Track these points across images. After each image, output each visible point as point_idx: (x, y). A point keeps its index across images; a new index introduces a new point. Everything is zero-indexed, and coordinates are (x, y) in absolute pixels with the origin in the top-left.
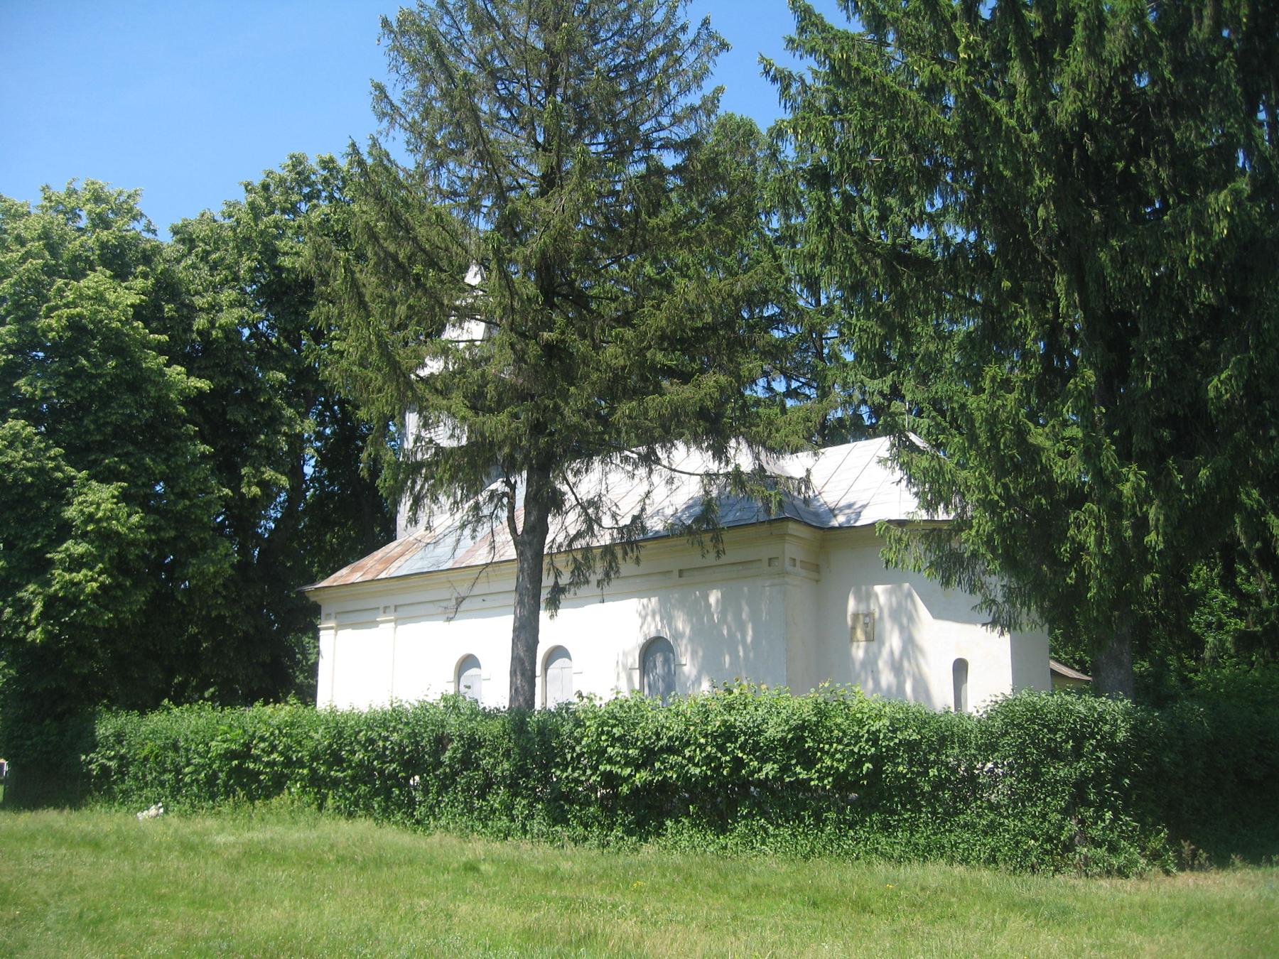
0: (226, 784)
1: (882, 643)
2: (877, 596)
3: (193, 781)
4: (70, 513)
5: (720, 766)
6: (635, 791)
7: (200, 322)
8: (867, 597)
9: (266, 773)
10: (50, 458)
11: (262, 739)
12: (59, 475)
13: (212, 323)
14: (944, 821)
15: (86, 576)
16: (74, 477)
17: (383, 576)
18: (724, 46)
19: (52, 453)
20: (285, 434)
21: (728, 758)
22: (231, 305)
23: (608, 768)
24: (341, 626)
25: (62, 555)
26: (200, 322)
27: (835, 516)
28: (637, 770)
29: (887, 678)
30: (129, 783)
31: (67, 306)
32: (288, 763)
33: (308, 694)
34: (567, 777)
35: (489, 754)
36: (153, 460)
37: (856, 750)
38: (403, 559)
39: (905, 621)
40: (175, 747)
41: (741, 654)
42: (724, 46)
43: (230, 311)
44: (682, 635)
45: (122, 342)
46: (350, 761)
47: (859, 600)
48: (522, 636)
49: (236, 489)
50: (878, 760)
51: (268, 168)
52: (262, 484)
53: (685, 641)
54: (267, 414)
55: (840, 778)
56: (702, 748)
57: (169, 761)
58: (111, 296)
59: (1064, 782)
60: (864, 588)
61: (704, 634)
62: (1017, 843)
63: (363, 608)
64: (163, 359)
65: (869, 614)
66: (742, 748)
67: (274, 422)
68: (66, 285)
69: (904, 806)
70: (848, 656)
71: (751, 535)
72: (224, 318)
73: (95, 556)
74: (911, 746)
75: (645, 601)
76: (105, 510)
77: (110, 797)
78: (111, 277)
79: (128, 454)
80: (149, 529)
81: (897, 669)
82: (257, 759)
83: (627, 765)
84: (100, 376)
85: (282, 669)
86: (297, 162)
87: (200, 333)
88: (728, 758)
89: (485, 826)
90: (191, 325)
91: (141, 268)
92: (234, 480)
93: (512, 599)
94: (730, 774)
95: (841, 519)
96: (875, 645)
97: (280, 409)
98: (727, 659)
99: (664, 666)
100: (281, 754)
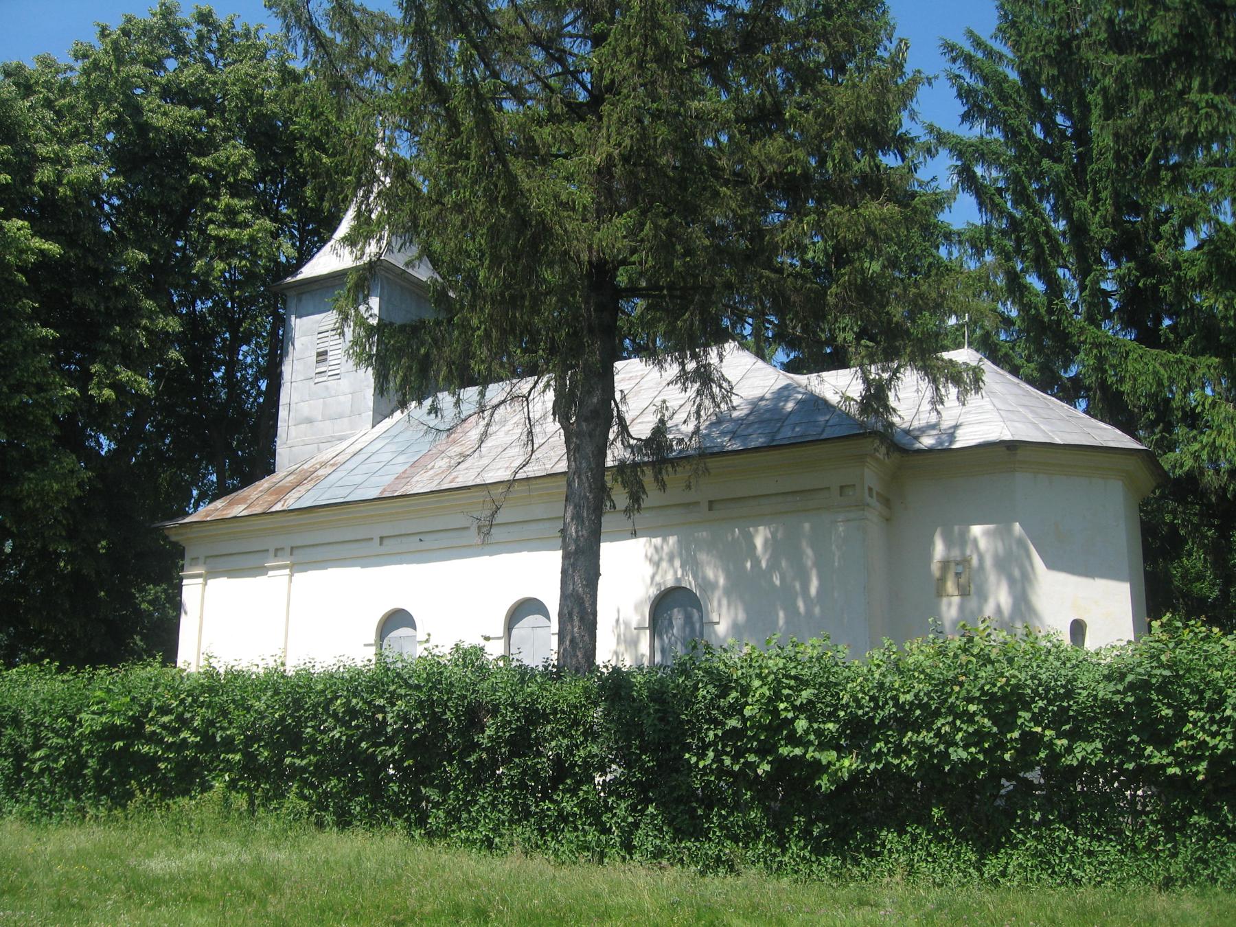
0: (97, 775)
1: (983, 597)
2: (975, 541)
3: (42, 771)
6: (844, 787)
7: (45, 174)
8: (959, 540)
11: (164, 710)
13: (59, 176)
20: (145, 328)
22: (81, 162)
24: (212, 574)
26: (45, 174)
32: (208, 743)
33: (170, 655)
38: (302, 489)
39: (1017, 573)
43: (87, 167)
46: (315, 742)
49: (84, 390)
52: (117, 386)
53: (718, 594)
54: (122, 303)
60: (956, 528)
63: (242, 553)
66: (1036, 720)
67: (130, 315)
82: (153, 739)
83: (822, 747)
86: (167, 12)
87: (42, 185)
90: (31, 177)
92: (83, 379)
95: (927, 441)
100: (195, 732)
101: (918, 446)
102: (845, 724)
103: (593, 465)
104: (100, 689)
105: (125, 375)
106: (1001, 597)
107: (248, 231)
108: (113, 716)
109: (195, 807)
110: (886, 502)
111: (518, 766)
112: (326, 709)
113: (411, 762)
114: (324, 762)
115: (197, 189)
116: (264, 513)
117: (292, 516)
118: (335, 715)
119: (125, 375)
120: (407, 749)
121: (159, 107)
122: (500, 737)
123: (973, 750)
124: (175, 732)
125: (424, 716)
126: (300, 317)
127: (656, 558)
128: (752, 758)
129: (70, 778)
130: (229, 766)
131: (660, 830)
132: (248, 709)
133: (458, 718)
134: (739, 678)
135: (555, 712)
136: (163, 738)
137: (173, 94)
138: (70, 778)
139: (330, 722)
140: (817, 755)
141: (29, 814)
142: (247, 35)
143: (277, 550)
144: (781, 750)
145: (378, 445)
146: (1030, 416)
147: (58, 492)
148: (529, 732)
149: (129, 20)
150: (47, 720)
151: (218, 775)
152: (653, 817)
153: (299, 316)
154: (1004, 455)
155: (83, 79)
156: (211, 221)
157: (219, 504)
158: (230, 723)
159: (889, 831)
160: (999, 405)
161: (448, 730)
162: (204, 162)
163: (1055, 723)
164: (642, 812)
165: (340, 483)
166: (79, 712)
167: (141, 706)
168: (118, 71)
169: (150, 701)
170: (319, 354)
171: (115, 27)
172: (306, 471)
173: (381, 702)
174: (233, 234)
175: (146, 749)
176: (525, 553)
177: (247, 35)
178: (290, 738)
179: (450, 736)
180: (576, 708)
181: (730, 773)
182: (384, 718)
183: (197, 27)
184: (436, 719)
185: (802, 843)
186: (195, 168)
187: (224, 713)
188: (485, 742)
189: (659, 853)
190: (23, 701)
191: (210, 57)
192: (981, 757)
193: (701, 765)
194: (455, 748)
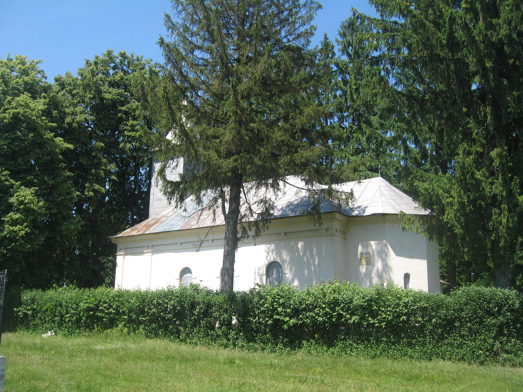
0: (85, 322)
1: (373, 266)
2: (371, 245)
3: (69, 321)
4: (13, 200)
5: (332, 317)
6: (290, 328)
7: (68, 119)
8: (367, 246)
10: (3, 175)
11: (105, 302)
12: (7, 183)
14: (438, 342)
15: (19, 228)
16: (14, 185)
18: (320, 7)
19: (4, 173)
20: (103, 170)
21: (336, 314)
22: (81, 113)
23: (278, 317)
24: (126, 254)
25: (8, 219)
26: (68, 119)
27: (353, 211)
28: (290, 319)
29: (375, 281)
30: (37, 321)
31: (12, 108)
32: (118, 313)
33: (112, 284)
34: (256, 321)
35: (217, 310)
36: (48, 178)
37: (398, 310)
38: (156, 225)
40: (61, 305)
41: (313, 269)
42: (320, 7)
43: (81, 115)
44: (286, 261)
45: (36, 126)
46: (148, 313)
47: (363, 247)
48: (228, 259)
50: (407, 314)
51: (97, 54)
52: (94, 191)
53: (287, 264)
55: (389, 323)
56: (324, 309)
57: (57, 311)
58: (32, 105)
59: (494, 325)
60: (365, 243)
61: (296, 261)
62: (473, 352)
63: (136, 247)
64: (52, 134)
65: (368, 254)
66: (342, 309)
68: (13, 99)
69: (419, 336)
70: (358, 271)
71: (323, 217)
72: (79, 118)
73: (23, 219)
74: (424, 309)
75: (269, 246)
76: (29, 199)
77: (28, 327)
78: (31, 97)
79: (37, 175)
80: (47, 209)
81: (380, 276)
82: (102, 311)
83: (286, 316)
84: (26, 140)
85: (97, 270)
86: (109, 53)
87: (68, 124)
88: (336, 314)
89: (215, 343)
90: (64, 121)
91: (43, 94)
92: (82, 189)
93: (223, 242)
94: (336, 321)
95: (356, 213)
96: (370, 267)
97: (100, 159)
98: (306, 271)
99: (277, 274)
100: (114, 309)
102: (293, 310)
105: (97, 187)
107: (139, 133)
109: (115, 331)
110: (344, 233)
111: (205, 320)
112: (151, 303)
115: (121, 118)
117: (152, 235)
119: (97, 187)
120: (176, 316)
121: (107, 90)
124: (108, 309)
125: (179, 305)
127: (268, 251)
129: (77, 323)
130: (124, 320)
132: (129, 302)
138: (77, 323)
141: (65, 334)
142: (138, 60)
146: (393, 203)
147: (74, 228)
148: (208, 311)
149: (97, 58)
150: (70, 305)
154: (381, 218)
155: (81, 82)
156: (126, 130)
157: (128, 230)
158: (124, 306)
160: (384, 200)
162: (124, 108)
163: (347, 311)
166: (80, 302)
168: (93, 79)
169: (101, 299)
171: (92, 60)
172: (158, 219)
174: (133, 134)
177: (138, 60)
178: (142, 312)
183: (120, 58)
184: (182, 306)
186: (120, 111)
188: (196, 314)
190: (63, 299)
191: (125, 68)
192: (326, 320)
193: (254, 321)
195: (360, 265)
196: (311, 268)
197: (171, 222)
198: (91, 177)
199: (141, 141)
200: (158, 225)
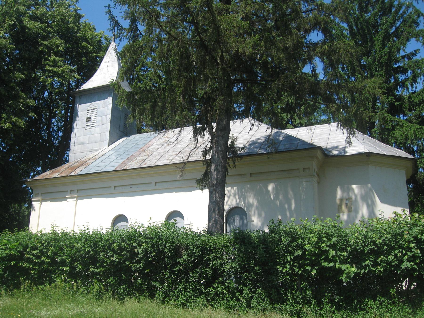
2: (353, 190)
8: (347, 189)
9: (35, 269)
11: (33, 249)
17: (73, 174)
20: (22, 103)
24: (44, 200)
32: (53, 263)
38: (82, 168)
39: (370, 202)
47: (343, 191)
53: (253, 209)
63: (57, 192)
65: (349, 199)
67: (16, 97)
82: (28, 260)
83: (342, 263)
95: (335, 152)
100: (48, 257)
101: (331, 154)
102: (351, 253)
103: (223, 149)
104: (5, 240)
106: (364, 211)
108: (11, 251)
111: (197, 272)
112: (109, 247)
113: (148, 270)
114: (106, 271)
115: (42, 52)
116: (67, 176)
117: (79, 178)
118: (113, 250)
119: (14, 119)
122: (189, 260)
123: (412, 263)
124: (39, 257)
126: (81, 104)
128: (308, 268)
131: (264, 300)
133: (170, 251)
134: (300, 234)
135: (215, 248)
136: (33, 260)
137: (33, 18)
139: (112, 253)
140: (340, 266)
143: (71, 191)
144: (323, 264)
145: (111, 152)
148: (203, 257)
151: (59, 276)
152: (260, 294)
153: (80, 104)
154: (367, 157)
156: (48, 64)
157: (48, 173)
158: (64, 254)
159: (368, 299)
161: (166, 257)
162: (45, 43)
164: (255, 292)
165: (98, 165)
167: (23, 246)
170: (88, 118)
172: (83, 161)
173: (135, 244)
175: (25, 265)
176: (174, 193)
179: (166, 259)
180: (225, 247)
181: (297, 275)
182: (137, 251)
185: (330, 305)
186: (42, 45)
187: (61, 249)
189: (264, 310)
192: (416, 267)
194: (168, 265)
195: (339, 212)
196: (286, 215)
197: (103, 164)
198: (8, 108)
199: (64, 77)
200: (85, 166)
